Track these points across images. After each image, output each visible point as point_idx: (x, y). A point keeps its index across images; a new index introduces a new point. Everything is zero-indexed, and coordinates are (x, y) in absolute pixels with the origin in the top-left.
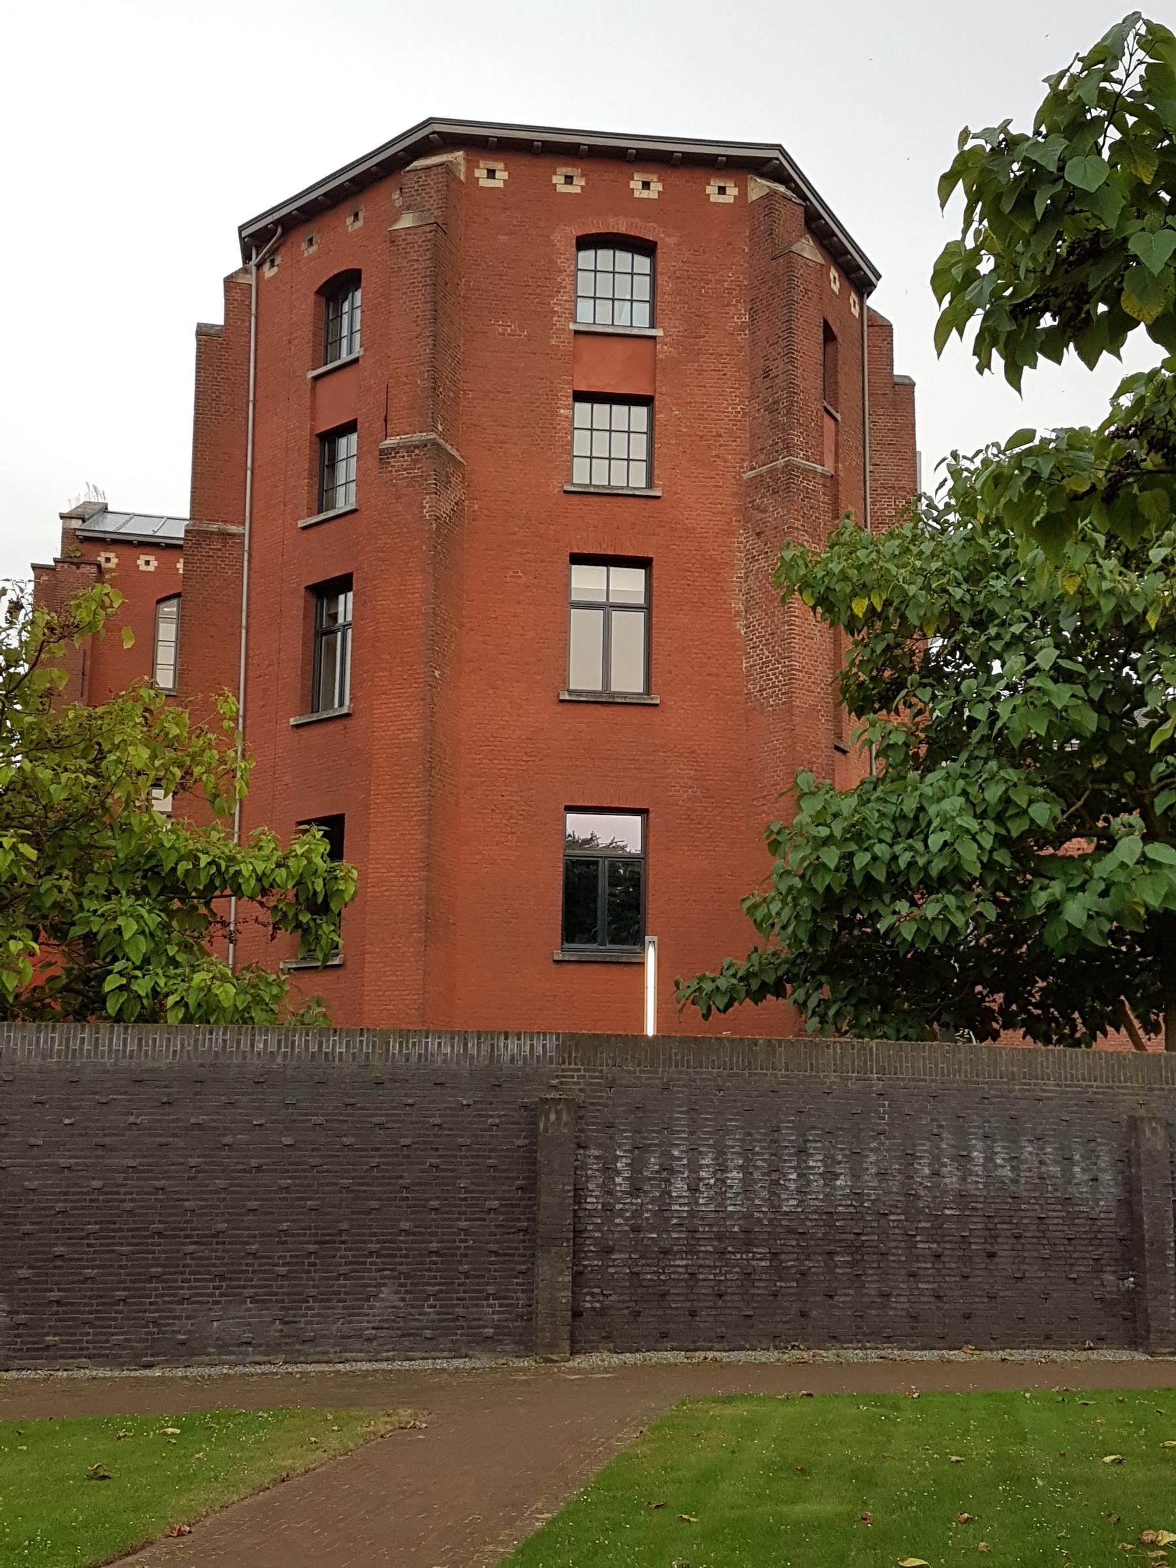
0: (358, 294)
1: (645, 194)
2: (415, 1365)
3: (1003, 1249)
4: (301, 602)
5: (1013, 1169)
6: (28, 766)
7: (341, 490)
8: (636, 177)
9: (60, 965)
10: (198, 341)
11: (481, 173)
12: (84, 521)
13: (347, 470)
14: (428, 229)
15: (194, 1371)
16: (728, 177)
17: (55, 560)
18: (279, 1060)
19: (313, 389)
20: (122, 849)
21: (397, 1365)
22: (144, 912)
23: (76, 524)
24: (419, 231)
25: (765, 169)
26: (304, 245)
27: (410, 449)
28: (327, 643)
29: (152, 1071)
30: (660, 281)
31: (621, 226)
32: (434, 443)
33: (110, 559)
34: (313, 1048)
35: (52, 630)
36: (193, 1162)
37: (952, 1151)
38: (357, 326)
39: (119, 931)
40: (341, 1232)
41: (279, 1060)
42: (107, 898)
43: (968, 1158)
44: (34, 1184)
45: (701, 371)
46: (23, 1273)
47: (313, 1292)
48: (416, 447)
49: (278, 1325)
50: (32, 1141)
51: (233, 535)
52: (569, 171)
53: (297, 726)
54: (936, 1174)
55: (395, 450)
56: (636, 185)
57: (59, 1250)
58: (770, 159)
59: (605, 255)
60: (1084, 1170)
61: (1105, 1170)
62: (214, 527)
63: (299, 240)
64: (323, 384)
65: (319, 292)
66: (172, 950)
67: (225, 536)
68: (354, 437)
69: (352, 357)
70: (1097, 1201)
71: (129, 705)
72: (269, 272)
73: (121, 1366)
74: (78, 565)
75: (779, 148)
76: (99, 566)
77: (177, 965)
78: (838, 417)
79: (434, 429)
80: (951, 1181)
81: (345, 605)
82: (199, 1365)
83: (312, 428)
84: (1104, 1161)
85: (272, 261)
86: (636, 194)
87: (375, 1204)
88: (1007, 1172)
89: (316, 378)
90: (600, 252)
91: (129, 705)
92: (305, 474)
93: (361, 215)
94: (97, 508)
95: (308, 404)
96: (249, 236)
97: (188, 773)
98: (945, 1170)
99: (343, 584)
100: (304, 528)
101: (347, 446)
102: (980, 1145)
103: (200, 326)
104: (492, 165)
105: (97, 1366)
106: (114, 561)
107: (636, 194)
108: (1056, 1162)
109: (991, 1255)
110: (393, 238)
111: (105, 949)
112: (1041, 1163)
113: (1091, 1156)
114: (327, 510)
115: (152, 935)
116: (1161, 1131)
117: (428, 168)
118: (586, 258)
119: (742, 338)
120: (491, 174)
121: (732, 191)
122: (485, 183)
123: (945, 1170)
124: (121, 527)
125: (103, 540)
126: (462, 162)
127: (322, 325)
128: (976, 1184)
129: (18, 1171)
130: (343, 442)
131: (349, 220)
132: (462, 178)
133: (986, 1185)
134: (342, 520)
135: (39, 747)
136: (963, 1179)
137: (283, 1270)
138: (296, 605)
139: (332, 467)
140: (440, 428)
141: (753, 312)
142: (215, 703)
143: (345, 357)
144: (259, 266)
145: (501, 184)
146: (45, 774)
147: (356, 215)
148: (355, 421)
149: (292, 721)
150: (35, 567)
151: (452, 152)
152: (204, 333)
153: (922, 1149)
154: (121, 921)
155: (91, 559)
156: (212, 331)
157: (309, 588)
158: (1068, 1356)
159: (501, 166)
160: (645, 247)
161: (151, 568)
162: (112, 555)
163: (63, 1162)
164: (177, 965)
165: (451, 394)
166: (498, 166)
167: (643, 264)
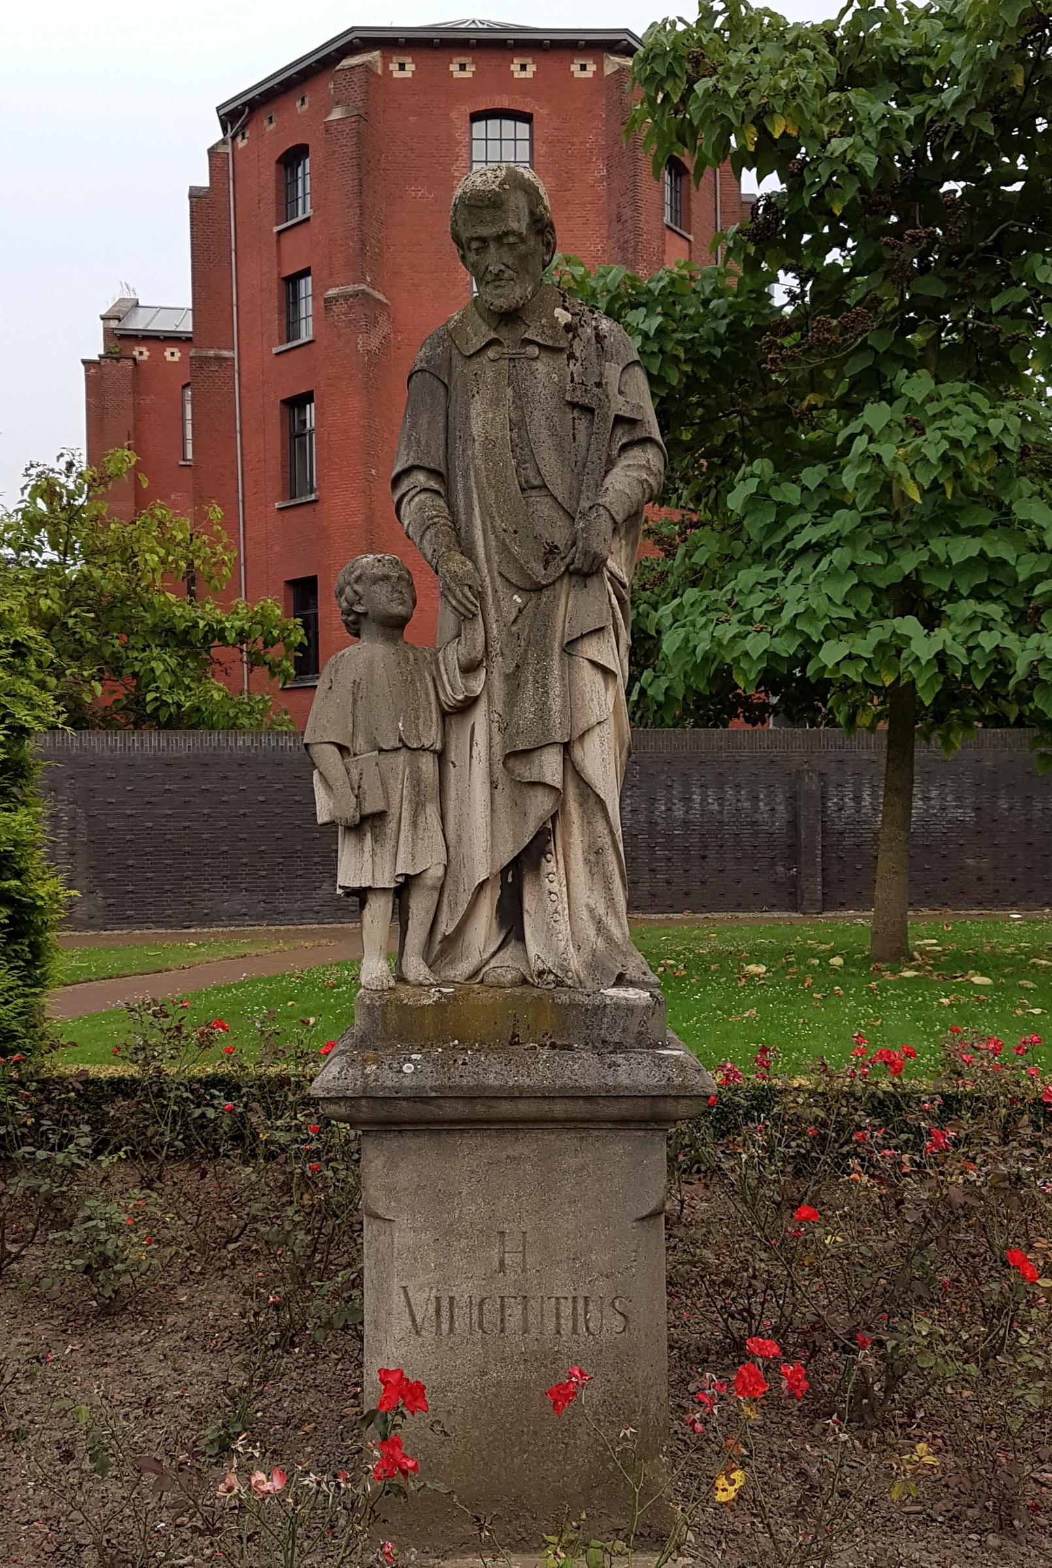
0: (308, 161)
1: (523, 75)
2: (345, 925)
3: (712, 854)
4: (277, 412)
5: (719, 805)
6: (85, 568)
7: (303, 322)
8: (515, 61)
9: (121, 693)
10: (191, 202)
11: (394, 67)
12: (120, 320)
13: (306, 307)
14: (353, 119)
15: (211, 930)
16: (585, 56)
17: (100, 356)
18: (253, 751)
19: (278, 241)
20: (149, 619)
21: (334, 925)
22: (166, 657)
23: (114, 324)
24: (347, 121)
25: (616, 48)
26: (266, 122)
27: (346, 297)
28: (300, 444)
29: (176, 758)
30: (535, 146)
31: (504, 102)
32: (363, 292)
33: (142, 353)
34: (273, 744)
35: (94, 480)
36: (206, 811)
37: (680, 796)
38: (308, 190)
39: (152, 670)
40: (296, 852)
41: (253, 751)
42: (144, 650)
43: (690, 799)
44: (112, 825)
45: (569, 218)
46: (111, 875)
47: (282, 885)
48: (351, 296)
49: (262, 904)
50: (109, 800)
51: (226, 359)
52: (463, 60)
53: (281, 509)
54: (669, 809)
55: (335, 299)
56: (515, 67)
57: (130, 862)
58: (620, 41)
59: (493, 124)
60: (766, 804)
61: (780, 804)
62: (211, 353)
63: (262, 115)
64: (285, 237)
65: (278, 162)
66: (187, 681)
67: (220, 359)
68: (309, 279)
69: (305, 216)
70: (774, 823)
71: (149, 521)
72: (241, 143)
73: (171, 927)
74: (118, 360)
75: (627, 31)
76: (134, 359)
77: (191, 690)
78: (691, 237)
79: (363, 281)
80: (679, 813)
81: (310, 411)
82: (217, 926)
83: (279, 274)
84: (780, 798)
85: (243, 134)
86: (516, 75)
87: (318, 835)
88: (716, 807)
89: (280, 232)
90: (489, 122)
91: (149, 521)
92: (276, 310)
93: (307, 100)
94: (130, 304)
95: (275, 254)
96: (225, 115)
97: (190, 564)
98: (674, 807)
99: (308, 397)
100: (277, 354)
101: (306, 286)
102: (698, 791)
103: (191, 188)
104: (402, 60)
105: (158, 928)
106: (146, 354)
107: (516, 75)
108: (748, 800)
109: (704, 857)
110: (328, 127)
111: (144, 681)
112: (738, 800)
113: (770, 795)
114: (294, 339)
115: (173, 672)
116: (815, 778)
117: (352, 68)
118: (479, 128)
119: (601, 189)
120: (402, 67)
121: (592, 68)
122: (398, 74)
123: (674, 807)
124: (148, 325)
125: (136, 337)
126: (380, 59)
127: (282, 187)
128: (695, 815)
129: (103, 818)
130: (303, 282)
131: (299, 103)
132: (380, 72)
133: (702, 815)
134: (302, 349)
135: (93, 553)
136: (687, 812)
137: (264, 873)
138: (275, 413)
139: (296, 303)
140: (368, 279)
141: (609, 168)
142: (207, 514)
143: (301, 217)
144: (234, 138)
145: (409, 75)
146: (97, 573)
147: (303, 100)
148: (309, 268)
149: (277, 505)
150: (84, 362)
151: (370, 52)
152: (196, 197)
153: (661, 794)
154: (153, 664)
155: (127, 354)
156: (201, 194)
157: (282, 401)
158: (746, 915)
159: (409, 60)
160: (527, 118)
161: (176, 359)
162: (144, 349)
163: (129, 812)
164: (191, 690)
165: (377, 250)
166: (407, 60)
167: (523, 129)
